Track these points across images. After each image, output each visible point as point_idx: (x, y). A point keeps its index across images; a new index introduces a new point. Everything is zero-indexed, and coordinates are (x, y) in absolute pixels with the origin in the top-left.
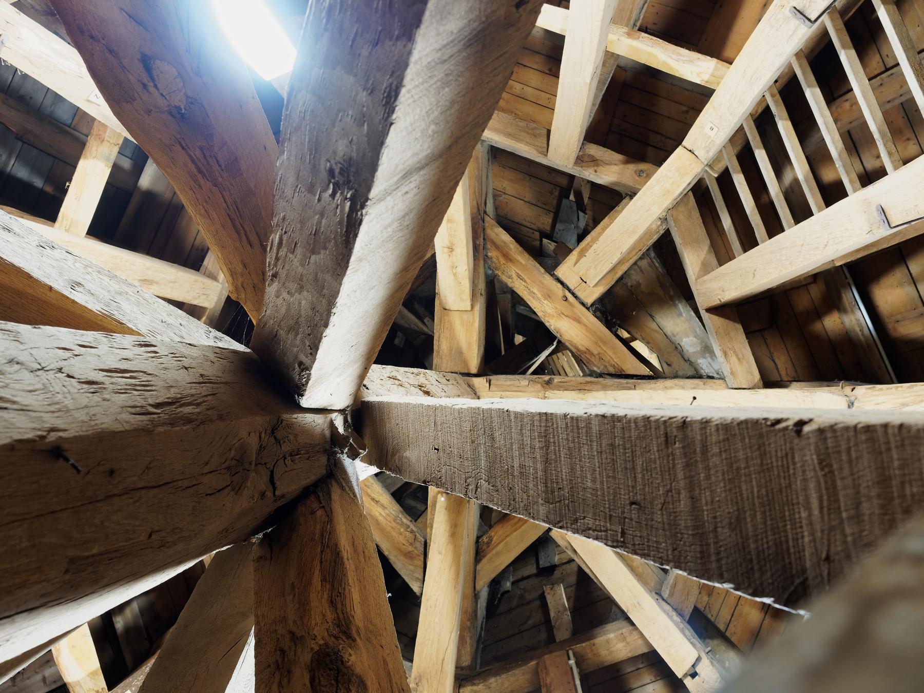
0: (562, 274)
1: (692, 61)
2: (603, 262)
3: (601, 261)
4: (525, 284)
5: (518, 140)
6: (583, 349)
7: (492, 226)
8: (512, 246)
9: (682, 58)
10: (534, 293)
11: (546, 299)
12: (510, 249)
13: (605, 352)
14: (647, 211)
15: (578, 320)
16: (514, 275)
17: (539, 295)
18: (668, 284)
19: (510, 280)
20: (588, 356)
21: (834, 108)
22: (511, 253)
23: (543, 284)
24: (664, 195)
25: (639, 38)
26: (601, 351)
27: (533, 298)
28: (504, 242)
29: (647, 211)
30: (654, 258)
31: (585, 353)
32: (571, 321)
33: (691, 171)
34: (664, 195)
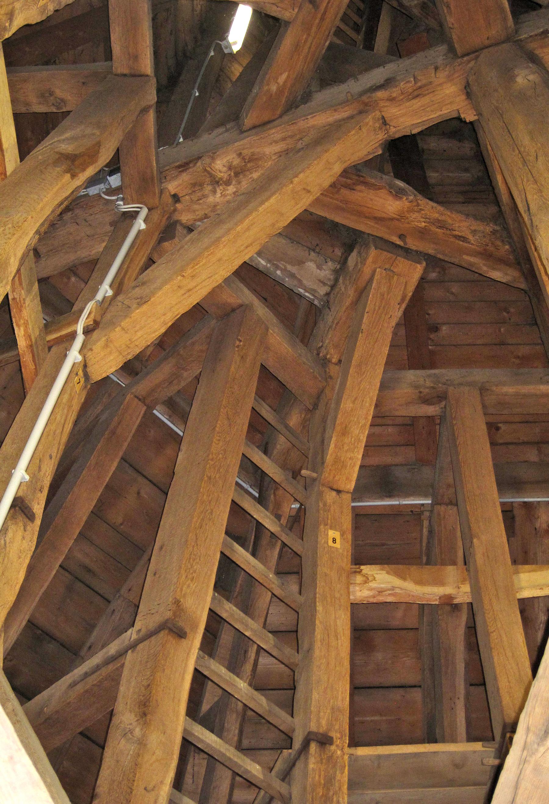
0: (417, 267)
1: (379, 592)
2: (377, 308)
3: (379, 308)
4: (454, 233)
5: (517, 394)
6: (359, 187)
7: (515, 281)
8: (485, 268)
9: (390, 592)
10: (440, 227)
11: (425, 228)
12: (484, 265)
13: (331, 198)
14: (356, 399)
15: (379, 220)
16: (471, 237)
17: (433, 229)
18: (287, 279)
19: (473, 228)
20: (349, 181)
21: (120, 371)
22: (484, 262)
23: (434, 243)
24: (346, 427)
25: (440, 598)
26: (336, 196)
27: (439, 220)
28: (494, 269)
29: (356, 399)
30: (314, 300)
31: (354, 184)
32: (384, 215)
33: (330, 470)
34: (346, 427)
